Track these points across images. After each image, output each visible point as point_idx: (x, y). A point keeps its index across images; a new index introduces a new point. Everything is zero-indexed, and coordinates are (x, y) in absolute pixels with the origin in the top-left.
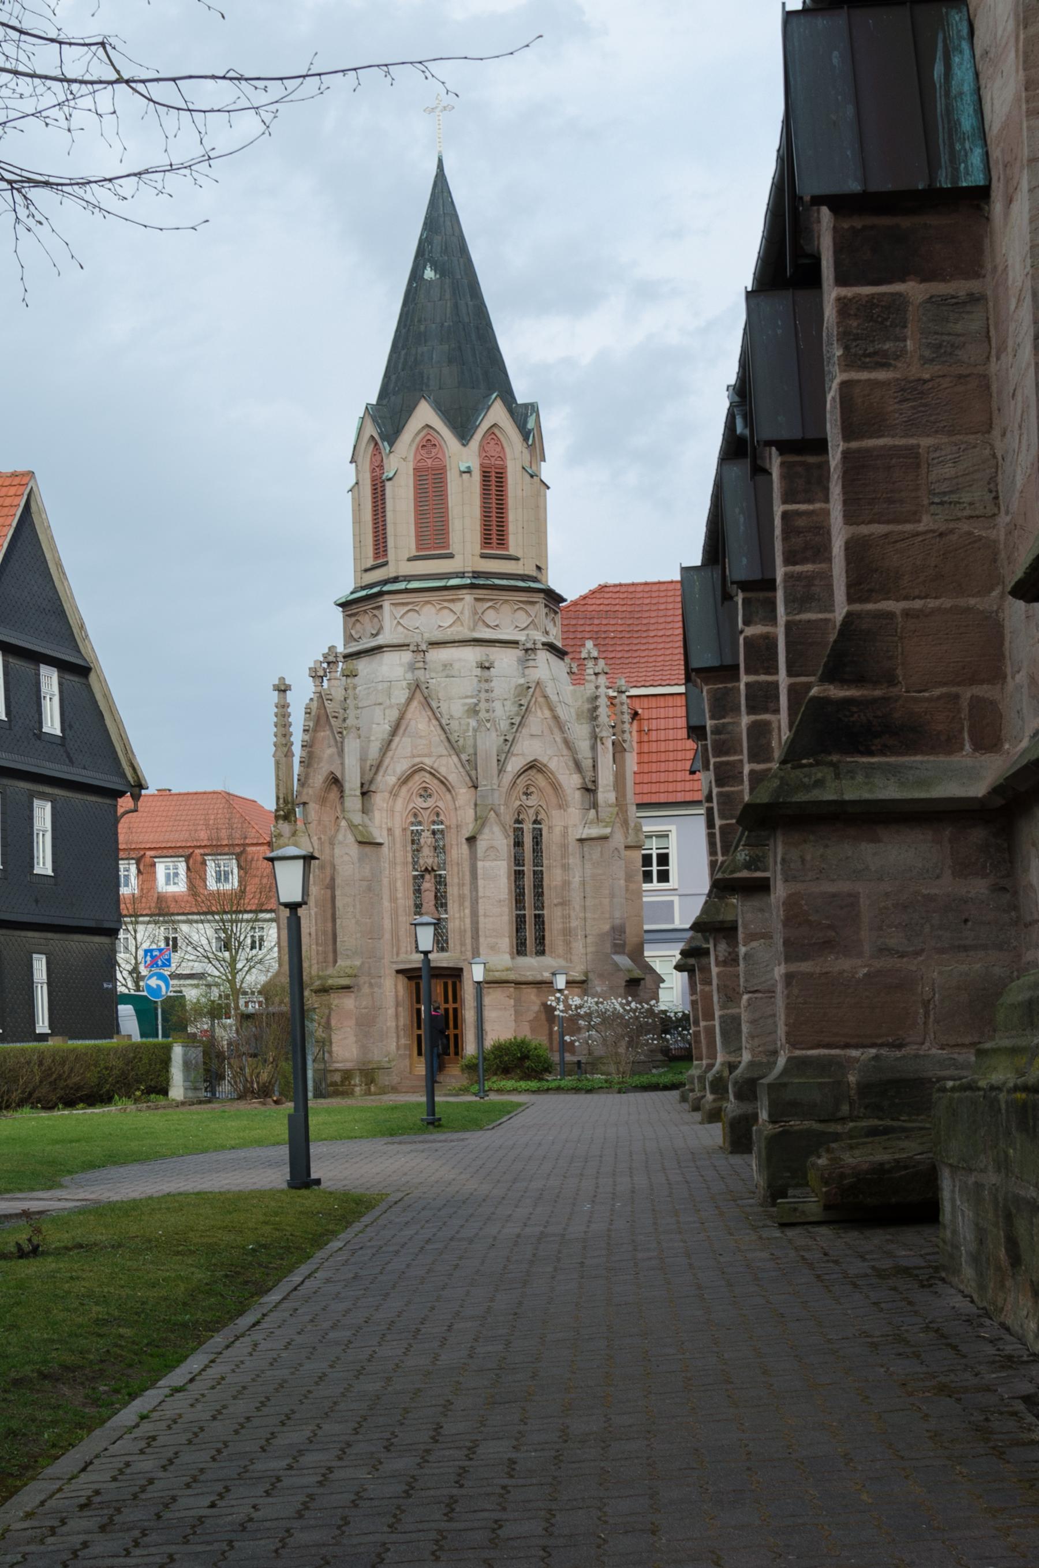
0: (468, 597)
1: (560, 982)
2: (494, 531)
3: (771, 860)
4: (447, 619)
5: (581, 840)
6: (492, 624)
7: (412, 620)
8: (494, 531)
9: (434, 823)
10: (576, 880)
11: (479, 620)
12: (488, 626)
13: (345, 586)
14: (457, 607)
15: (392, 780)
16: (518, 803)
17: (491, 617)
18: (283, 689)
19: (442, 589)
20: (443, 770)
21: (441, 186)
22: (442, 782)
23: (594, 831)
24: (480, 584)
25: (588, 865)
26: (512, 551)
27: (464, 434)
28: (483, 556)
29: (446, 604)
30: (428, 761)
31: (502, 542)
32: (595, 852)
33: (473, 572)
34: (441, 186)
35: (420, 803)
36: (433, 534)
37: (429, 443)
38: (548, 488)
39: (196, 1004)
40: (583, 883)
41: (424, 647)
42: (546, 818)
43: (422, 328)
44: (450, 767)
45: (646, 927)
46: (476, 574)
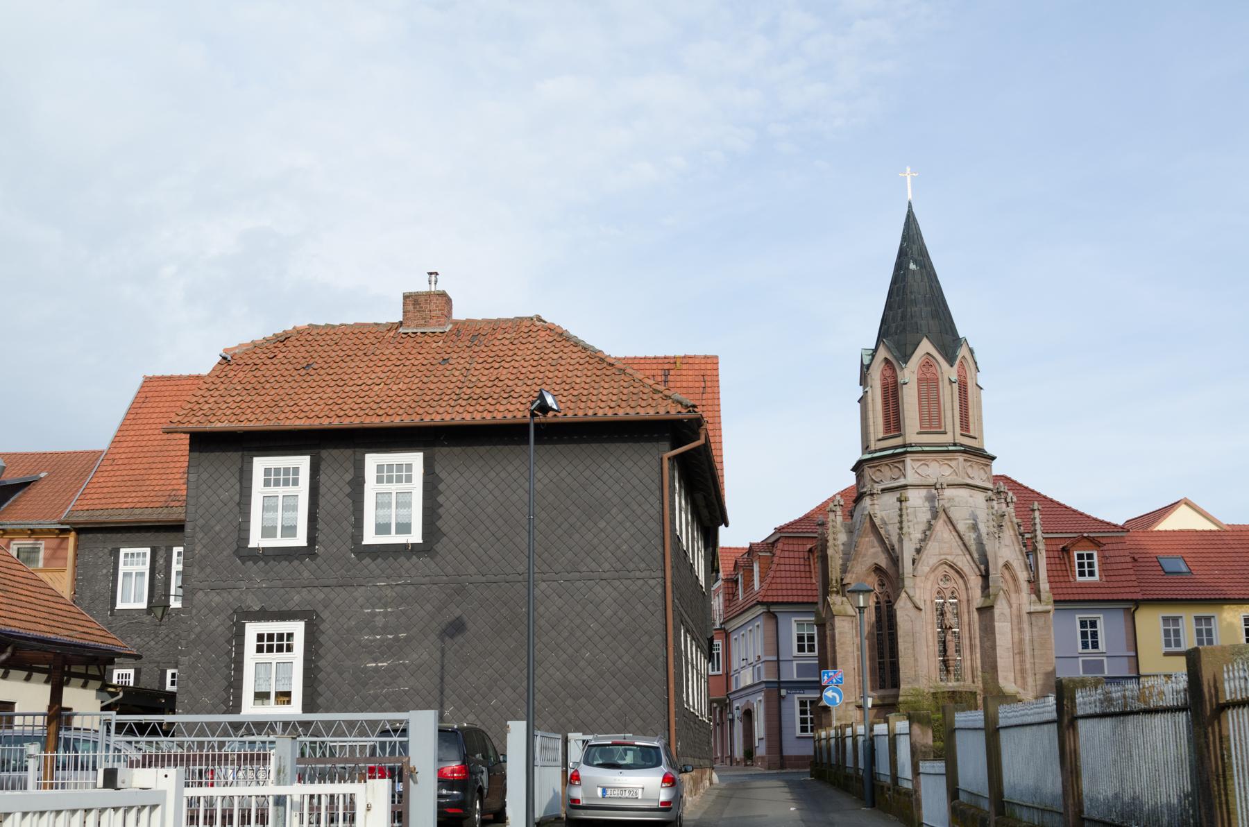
0: (961, 458)
2: (965, 424)
3: (977, 626)
4: (947, 471)
5: (1029, 613)
7: (924, 470)
8: (965, 424)
10: (1027, 638)
13: (857, 455)
14: (953, 463)
15: (927, 569)
19: (944, 452)
20: (960, 564)
22: (958, 572)
23: (1039, 608)
25: (1035, 629)
26: (972, 434)
27: (951, 360)
30: (949, 558)
31: (968, 429)
32: (1041, 621)
36: (932, 423)
37: (928, 363)
39: (1129, 805)
40: (1032, 641)
44: (964, 563)
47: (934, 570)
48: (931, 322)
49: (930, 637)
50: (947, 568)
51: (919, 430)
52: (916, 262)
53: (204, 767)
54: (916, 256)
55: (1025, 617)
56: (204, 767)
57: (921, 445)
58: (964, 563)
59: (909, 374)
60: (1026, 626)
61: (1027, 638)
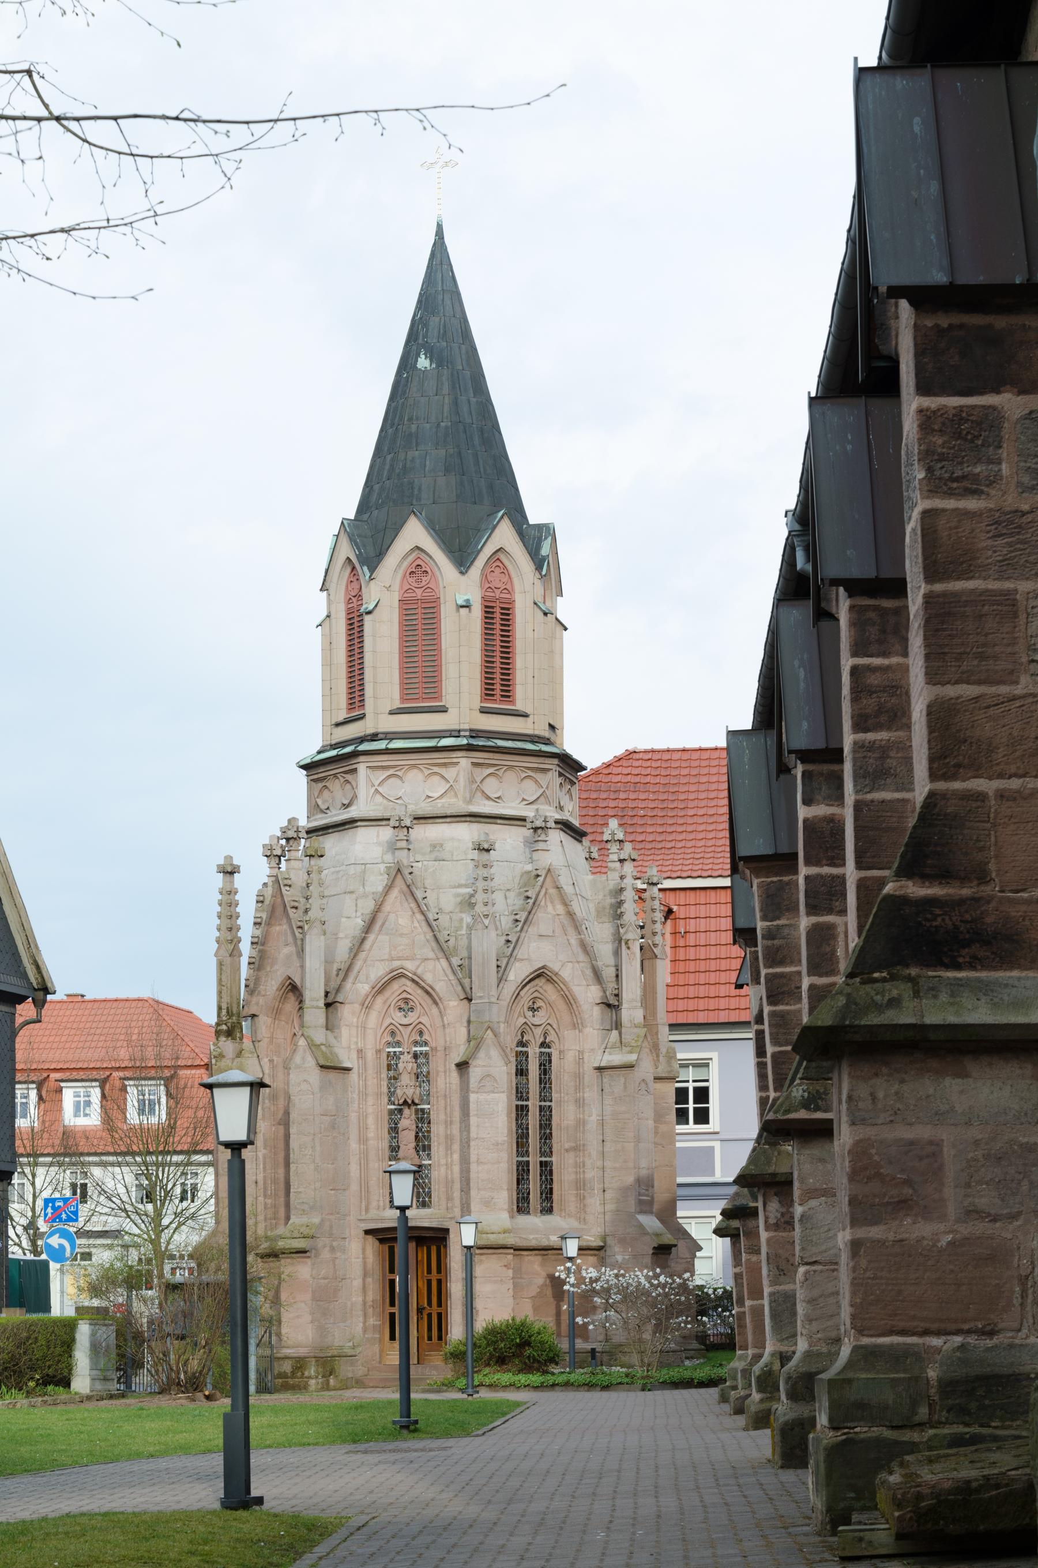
0: (464, 761)
1: (572, 1248)
2: (498, 680)
4: (436, 788)
5: (599, 1069)
6: (493, 796)
7: (393, 788)
8: (498, 680)
9: (416, 1043)
10: (593, 1118)
11: (477, 790)
12: (488, 798)
14: (450, 773)
16: (522, 1020)
17: (491, 786)
18: (229, 871)
19: (432, 750)
20: (429, 978)
21: (439, 261)
23: (616, 1058)
24: (478, 745)
25: (608, 1101)
26: (519, 706)
28: (484, 711)
29: (436, 769)
30: (409, 965)
31: (507, 694)
32: (616, 1083)
33: (471, 730)
34: (439, 261)
35: (398, 1017)
37: (418, 569)
38: (566, 629)
39: (108, 1269)
40: (602, 1123)
41: (407, 822)
42: (556, 1040)
43: (414, 428)
44: (437, 974)
45: (680, 1180)
46: (475, 733)
47: (381, 989)
48: (441, 481)
49: (371, 1121)
50: (410, 986)
51: (397, 704)
52: (431, 355)
53: (419, 627)
54: (432, 340)
55: (590, 1076)
56: (419, 627)
57: (390, 736)
58: (437, 974)
59: (384, 589)
60: (591, 1094)
61: (593, 1118)
